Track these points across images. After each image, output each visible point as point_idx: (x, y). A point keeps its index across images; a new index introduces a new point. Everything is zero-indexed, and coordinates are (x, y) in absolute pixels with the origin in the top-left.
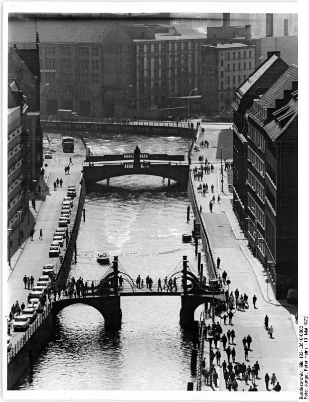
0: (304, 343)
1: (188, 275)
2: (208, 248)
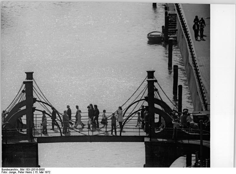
0: (34, 171)
1: (156, 106)
2: (190, 56)
